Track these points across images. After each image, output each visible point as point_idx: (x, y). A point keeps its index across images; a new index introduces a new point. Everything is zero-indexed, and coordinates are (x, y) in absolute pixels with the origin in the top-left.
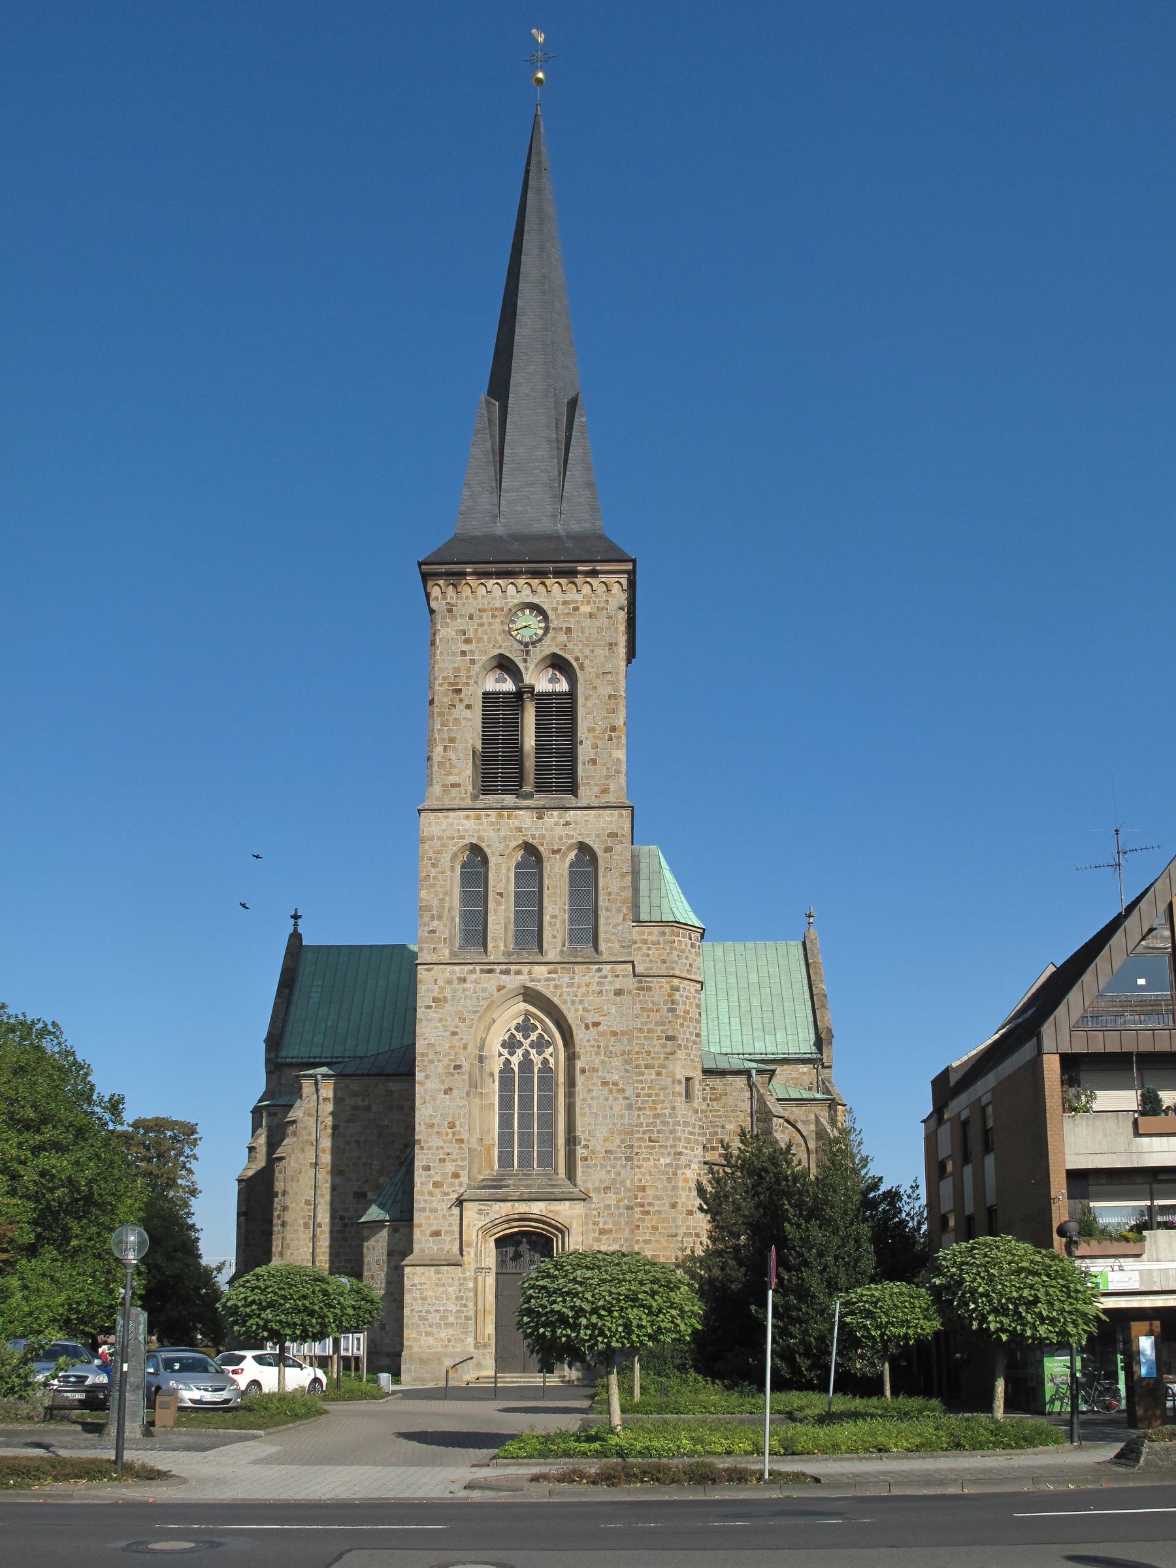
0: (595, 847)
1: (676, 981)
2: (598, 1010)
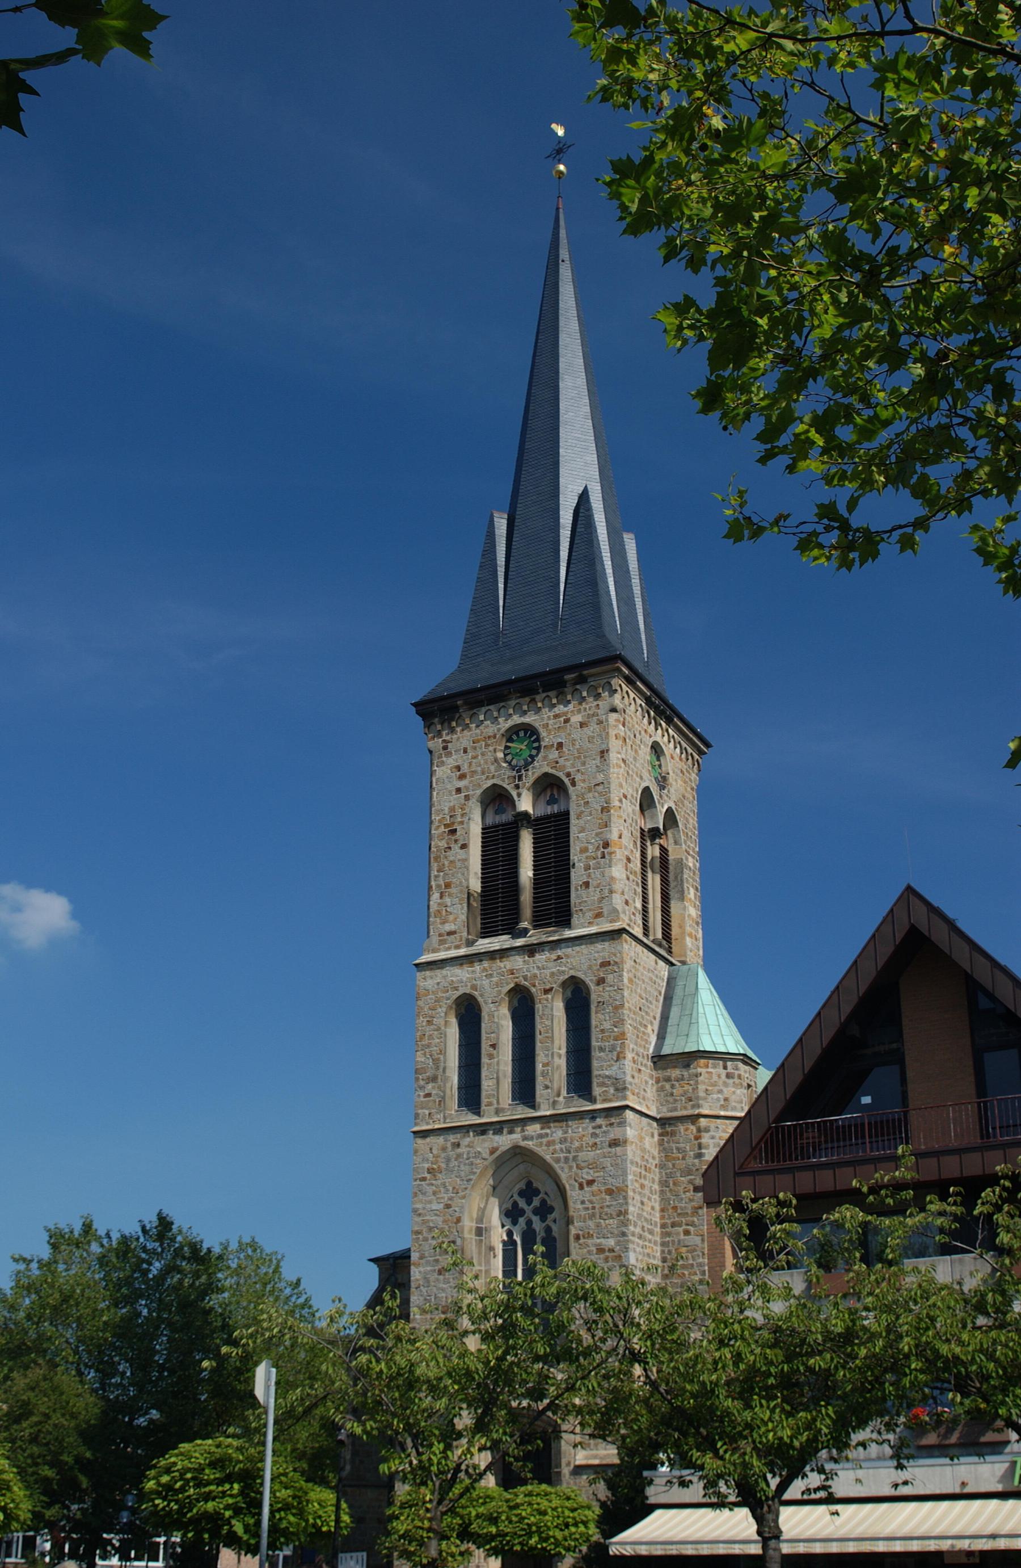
0: (587, 980)
1: (703, 1122)
2: (593, 1166)
